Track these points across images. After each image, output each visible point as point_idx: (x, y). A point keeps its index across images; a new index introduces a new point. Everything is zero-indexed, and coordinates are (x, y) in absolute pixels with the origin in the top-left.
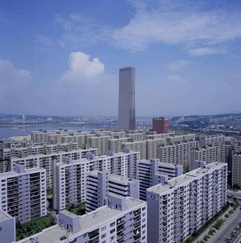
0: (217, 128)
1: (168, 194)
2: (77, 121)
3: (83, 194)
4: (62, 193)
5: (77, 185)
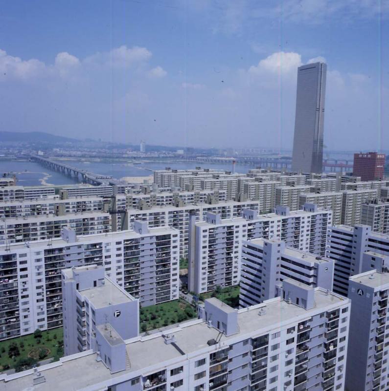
2: (222, 156)
4: (203, 269)
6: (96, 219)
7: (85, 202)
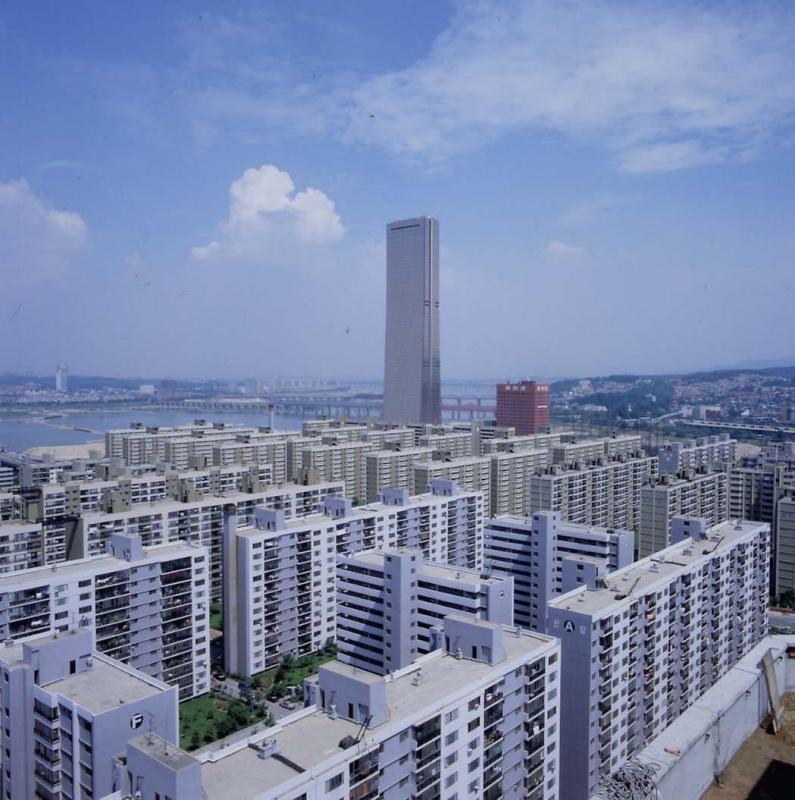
0: (699, 415)
1: (615, 615)
2: (238, 395)
3: (317, 624)
4: (255, 622)
5: (300, 598)
6: (11, 538)
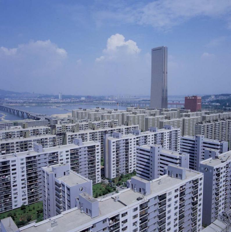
2: (108, 100)
4: (113, 164)
5: (126, 158)
7: (38, 129)
